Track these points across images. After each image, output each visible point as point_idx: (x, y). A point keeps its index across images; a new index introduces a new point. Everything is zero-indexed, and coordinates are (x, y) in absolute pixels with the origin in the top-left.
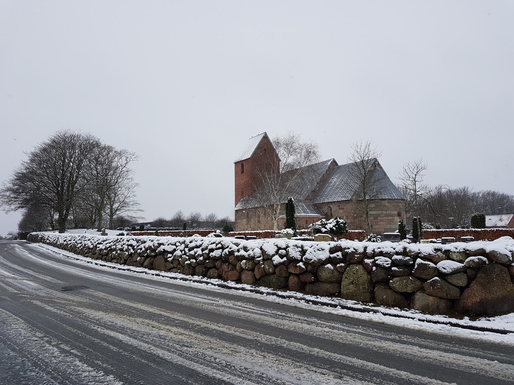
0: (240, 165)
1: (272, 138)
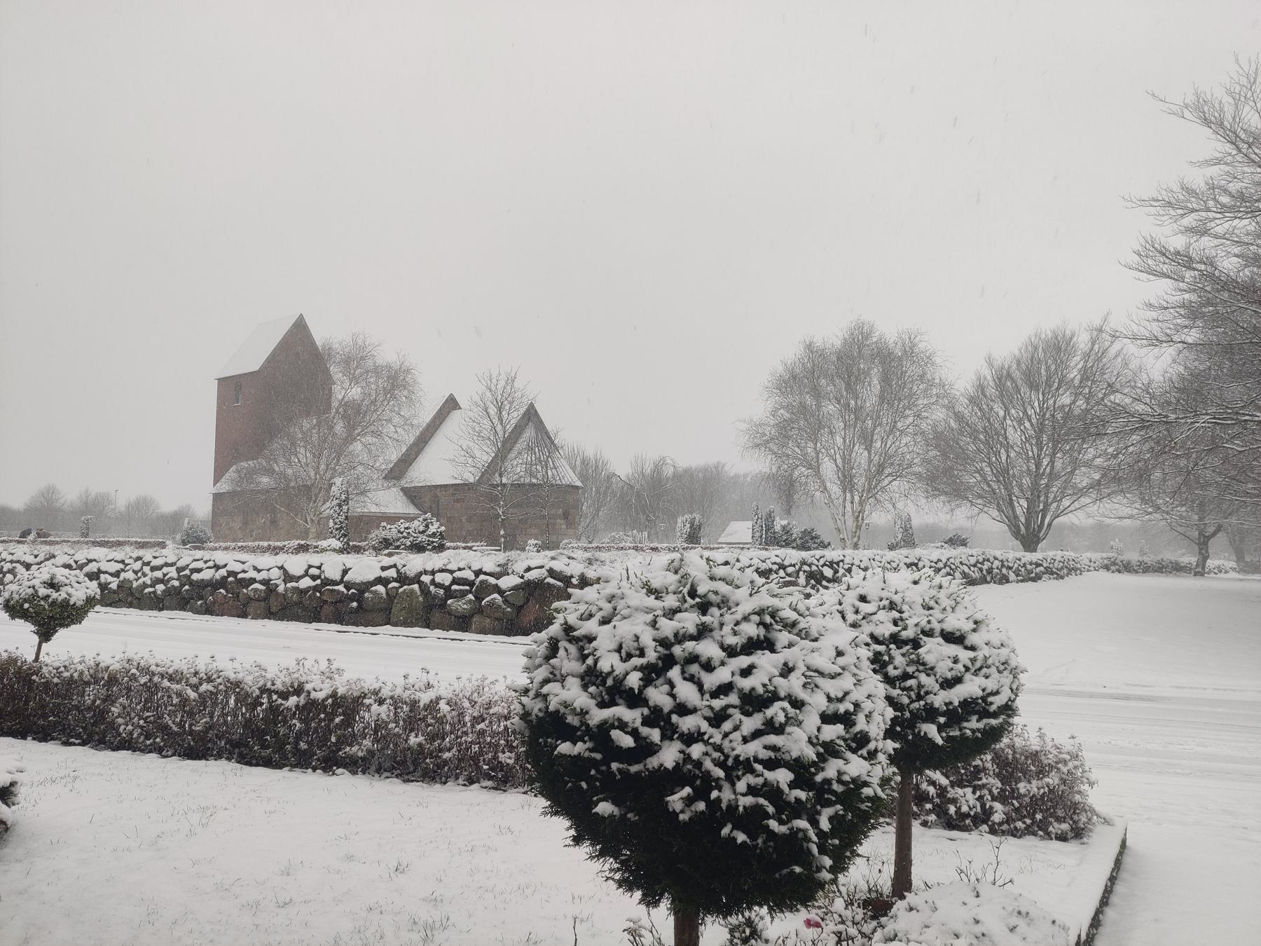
0: (231, 387)
1: (320, 334)
